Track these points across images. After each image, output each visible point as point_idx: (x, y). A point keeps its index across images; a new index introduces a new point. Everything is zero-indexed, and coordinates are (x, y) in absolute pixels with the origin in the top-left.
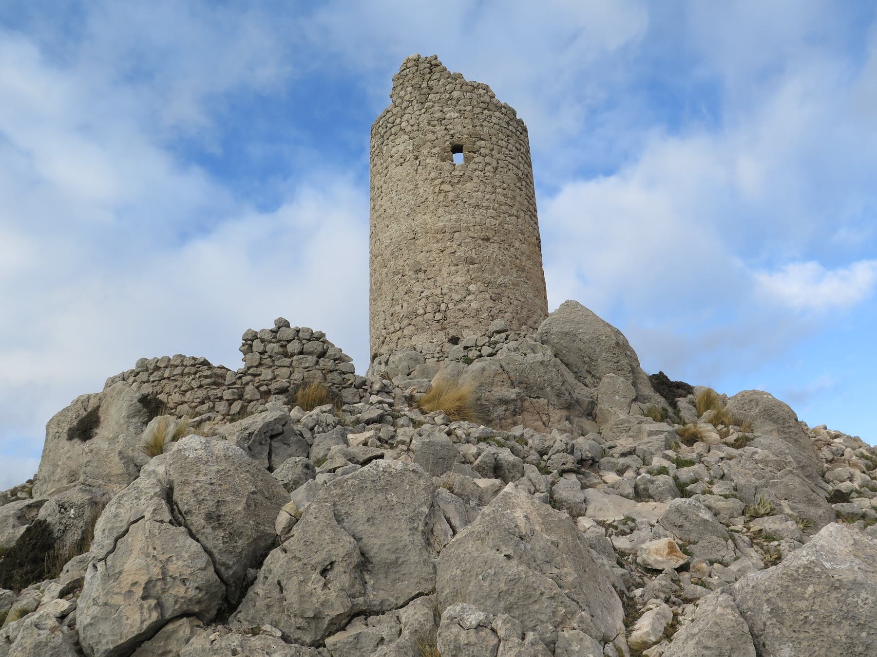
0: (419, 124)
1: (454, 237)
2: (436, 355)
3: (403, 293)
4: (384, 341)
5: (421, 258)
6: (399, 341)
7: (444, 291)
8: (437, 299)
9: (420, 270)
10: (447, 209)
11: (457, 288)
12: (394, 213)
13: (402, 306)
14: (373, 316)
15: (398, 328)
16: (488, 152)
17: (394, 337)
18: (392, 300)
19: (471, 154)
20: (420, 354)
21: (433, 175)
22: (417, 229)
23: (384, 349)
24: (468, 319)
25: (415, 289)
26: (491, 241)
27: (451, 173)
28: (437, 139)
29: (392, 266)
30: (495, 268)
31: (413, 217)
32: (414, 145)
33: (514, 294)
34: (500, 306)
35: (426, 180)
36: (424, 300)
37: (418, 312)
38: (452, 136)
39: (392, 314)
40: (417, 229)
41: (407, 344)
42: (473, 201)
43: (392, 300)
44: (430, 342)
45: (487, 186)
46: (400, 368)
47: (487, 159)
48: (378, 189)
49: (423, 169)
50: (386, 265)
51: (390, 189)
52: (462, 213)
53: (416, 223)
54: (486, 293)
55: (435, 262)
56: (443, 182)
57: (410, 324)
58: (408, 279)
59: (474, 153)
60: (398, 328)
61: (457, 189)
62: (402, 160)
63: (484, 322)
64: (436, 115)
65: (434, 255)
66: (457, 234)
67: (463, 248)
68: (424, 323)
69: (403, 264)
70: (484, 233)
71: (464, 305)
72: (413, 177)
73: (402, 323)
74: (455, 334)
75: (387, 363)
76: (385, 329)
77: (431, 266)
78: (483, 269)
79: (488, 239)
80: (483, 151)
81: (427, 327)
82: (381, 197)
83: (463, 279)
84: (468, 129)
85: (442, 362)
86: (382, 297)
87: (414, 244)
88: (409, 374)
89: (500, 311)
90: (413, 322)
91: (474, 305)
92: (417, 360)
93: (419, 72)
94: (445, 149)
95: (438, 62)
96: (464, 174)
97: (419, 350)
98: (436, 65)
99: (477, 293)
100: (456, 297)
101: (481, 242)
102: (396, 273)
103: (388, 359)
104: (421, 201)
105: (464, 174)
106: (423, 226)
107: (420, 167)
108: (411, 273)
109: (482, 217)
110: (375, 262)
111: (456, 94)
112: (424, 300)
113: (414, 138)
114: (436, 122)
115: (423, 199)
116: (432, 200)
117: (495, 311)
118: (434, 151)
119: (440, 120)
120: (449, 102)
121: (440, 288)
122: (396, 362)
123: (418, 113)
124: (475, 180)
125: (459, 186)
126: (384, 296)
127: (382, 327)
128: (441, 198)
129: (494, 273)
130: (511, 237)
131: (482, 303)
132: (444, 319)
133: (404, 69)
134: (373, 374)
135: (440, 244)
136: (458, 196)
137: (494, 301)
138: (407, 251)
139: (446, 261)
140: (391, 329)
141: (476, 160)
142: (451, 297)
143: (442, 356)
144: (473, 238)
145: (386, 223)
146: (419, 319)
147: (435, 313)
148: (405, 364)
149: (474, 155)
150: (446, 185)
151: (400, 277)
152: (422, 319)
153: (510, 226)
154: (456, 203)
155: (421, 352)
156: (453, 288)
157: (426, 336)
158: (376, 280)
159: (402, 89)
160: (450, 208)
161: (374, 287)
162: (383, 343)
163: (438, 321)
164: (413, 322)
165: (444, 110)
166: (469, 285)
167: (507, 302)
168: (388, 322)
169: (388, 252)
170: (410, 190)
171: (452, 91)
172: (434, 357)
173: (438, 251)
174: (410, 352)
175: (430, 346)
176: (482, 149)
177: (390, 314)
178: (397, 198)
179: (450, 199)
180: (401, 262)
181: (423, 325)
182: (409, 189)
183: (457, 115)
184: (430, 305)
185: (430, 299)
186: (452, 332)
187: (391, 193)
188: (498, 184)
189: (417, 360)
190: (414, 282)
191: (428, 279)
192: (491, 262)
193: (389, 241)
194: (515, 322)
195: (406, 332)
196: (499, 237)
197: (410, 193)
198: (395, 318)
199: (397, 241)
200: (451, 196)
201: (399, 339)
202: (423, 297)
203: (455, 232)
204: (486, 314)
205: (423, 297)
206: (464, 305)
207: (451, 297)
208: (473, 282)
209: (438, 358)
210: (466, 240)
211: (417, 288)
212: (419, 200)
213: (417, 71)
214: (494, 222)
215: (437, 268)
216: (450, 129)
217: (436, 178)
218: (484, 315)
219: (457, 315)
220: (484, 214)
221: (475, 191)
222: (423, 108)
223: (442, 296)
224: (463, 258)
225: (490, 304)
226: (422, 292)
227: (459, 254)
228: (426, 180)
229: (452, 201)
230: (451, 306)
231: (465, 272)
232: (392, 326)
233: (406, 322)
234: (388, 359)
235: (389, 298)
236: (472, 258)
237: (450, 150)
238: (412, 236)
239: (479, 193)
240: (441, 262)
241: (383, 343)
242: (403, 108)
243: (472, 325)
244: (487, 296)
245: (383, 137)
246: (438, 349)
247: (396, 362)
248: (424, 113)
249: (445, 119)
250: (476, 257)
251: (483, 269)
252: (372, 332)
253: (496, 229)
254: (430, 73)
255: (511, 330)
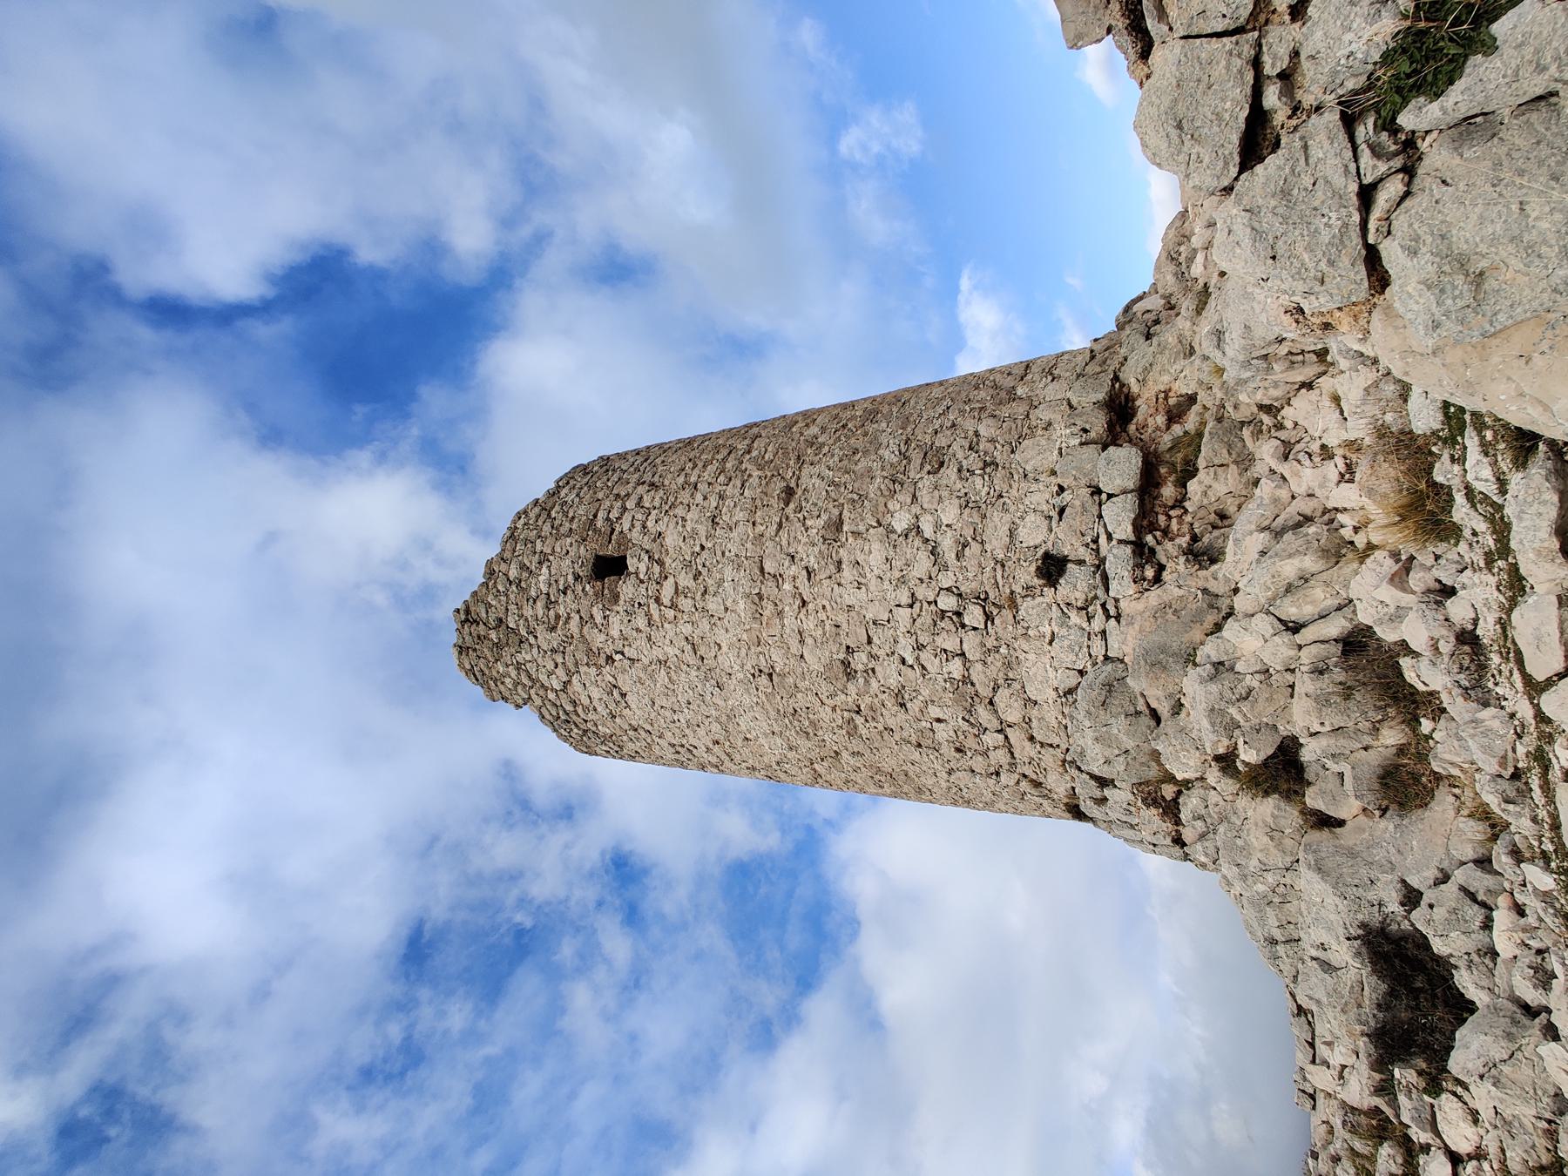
0: (554, 651)
1: (772, 572)
2: (1098, 623)
3: (902, 716)
4: (1032, 781)
5: (816, 660)
6: (1038, 738)
7: (905, 599)
8: (926, 619)
9: (846, 664)
10: (711, 590)
11: (898, 564)
12: (717, 720)
13: (939, 720)
14: (960, 799)
15: (1001, 737)
16: (619, 504)
17: (1024, 750)
18: (919, 746)
19: (614, 537)
20: (1090, 676)
21: (641, 622)
22: (748, 666)
23: (1058, 784)
24: (989, 531)
25: (893, 682)
26: (793, 484)
27: (642, 582)
28: (578, 612)
29: (834, 737)
30: (856, 468)
31: (723, 674)
32: (587, 664)
33: (930, 421)
34: (958, 449)
35: (650, 640)
36: (925, 656)
37: (957, 675)
38: (577, 578)
39: (958, 750)
40: (748, 666)
41: (1051, 714)
42: (702, 530)
43: (919, 746)
44: (1050, 643)
45: (679, 501)
46: (1129, 744)
47: (630, 504)
48: (678, 753)
49: (630, 645)
50: (833, 755)
51: (672, 725)
52: (723, 553)
53: (737, 667)
54: (920, 485)
55: (828, 623)
56: (658, 600)
57: (991, 703)
58: (868, 700)
59: (613, 530)
60: (1001, 737)
61: (673, 565)
62: (616, 692)
63: (999, 484)
64: (540, 613)
65: (810, 624)
66: (769, 567)
67: (799, 549)
68: (989, 660)
69: (828, 710)
70: (774, 502)
71: (947, 544)
72: (645, 669)
73: (985, 725)
74: (1033, 568)
75: (1103, 782)
76: (998, 774)
77: (838, 634)
78: (856, 497)
79: (789, 493)
80: (614, 514)
81: (1003, 650)
82: (691, 748)
83: (876, 546)
84: (571, 545)
85: (1122, 604)
86: (911, 774)
87: (782, 676)
88: (1155, 716)
89: (971, 448)
90: (985, 692)
91: (950, 513)
92: (1111, 685)
93: (477, 647)
94: (596, 595)
95: (464, 607)
96: (647, 552)
97: (1073, 680)
98: (468, 611)
99: (916, 509)
100: (923, 564)
101: (792, 506)
102: (852, 732)
103: (1093, 777)
104: (691, 652)
105: (647, 552)
106: (743, 651)
107: (626, 650)
108: (852, 688)
109: (738, 508)
110: (828, 778)
111: (513, 573)
112: (925, 656)
113: (577, 663)
114: (552, 613)
115: (688, 648)
116: (689, 626)
117: (973, 461)
118: (599, 619)
119: (549, 604)
120: (523, 584)
121: (895, 610)
122: (1108, 753)
123: (535, 650)
124: (661, 527)
125: (668, 561)
126: (911, 769)
127: (992, 782)
128: (685, 604)
129: (870, 470)
130: (794, 444)
131: (945, 494)
132: (982, 599)
133: (475, 675)
134: (1132, 827)
135: (787, 609)
136: (687, 565)
137: (942, 464)
138: (799, 695)
139: (828, 594)
140: (1001, 757)
141: (626, 526)
142: (921, 580)
143: (1103, 605)
144: (780, 525)
145: (740, 743)
146: (977, 673)
147: (963, 626)
148: (1119, 726)
149: (616, 533)
150: (663, 592)
151: (862, 720)
152: (979, 666)
153: (770, 449)
154: (700, 568)
155: (1081, 673)
156: (897, 574)
157: (1031, 657)
158: (870, 782)
159: (502, 683)
160: (710, 582)
161: (887, 790)
162: (1037, 784)
163: (989, 617)
164: (985, 692)
165: (533, 594)
166: (894, 531)
167: (949, 433)
168: (978, 763)
169: (802, 743)
170: (670, 678)
171: (508, 579)
172: (1104, 632)
173: (802, 616)
174: (1082, 705)
175: (1067, 643)
176: (611, 516)
177: (958, 755)
178: (686, 710)
179: (691, 584)
180: (825, 714)
181: (996, 662)
182: (667, 680)
183: (544, 570)
184: (939, 640)
185: (924, 639)
186: (1026, 574)
187: (678, 724)
188: (681, 480)
189: (1111, 685)
190: (874, 684)
191: (870, 641)
192: (843, 480)
193: (779, 741)
194: (1005, 411)
195: (1013, 716)
196: (788, 466)
197: (675, 678)
198: (970, 743)
199: (776, 720)
200: (685, 580)
201: (1032, 738)
202: (917, 658)
203: (762, 570)
204: (978, 481)
205: (917, 658)
206: (947, 544)
207: (921, 580)
208: (886, 520)
209: (1108, 617)
210: (784, 543)
211: (889, 674)
212: (689, 657)
213: (475, 650)
214: (754, 481)
215: (841, 618)
216: (565, 582)
217: (648, 615)
218: (979, 487)
219: (974, 562)
220: (732, 504)
221: (684, 526)
222: (527, 639)
223: (917, 605)
224: (824, 548)
225: (950, 473)
226: (903, 661)
227: (812, 559)
228: (650, 640)
229: (695, 578)
230: (946, 580)
231: (860, 541)
232: (991, 754)
233: (983, 714)
234: (1093, 777)
235: (916, 756)
236: (827, 526)
237: (599, 583)
238: (764, 680)
239: (688, 518)
240: (828, 607)
241: (1037, 784)
242: (530, 684)
243: (1007, 518)
244: (928, 481)
245: (585, 732)
246: (1076, 618)
247: (1108, 753)
248: (536, 637)
249: (548, 594)
250: (824, 517)
251: (856, 497)
252: (1003, 808)
253: (769, 474)
254: (478, 624)
255: (1028, 416)
